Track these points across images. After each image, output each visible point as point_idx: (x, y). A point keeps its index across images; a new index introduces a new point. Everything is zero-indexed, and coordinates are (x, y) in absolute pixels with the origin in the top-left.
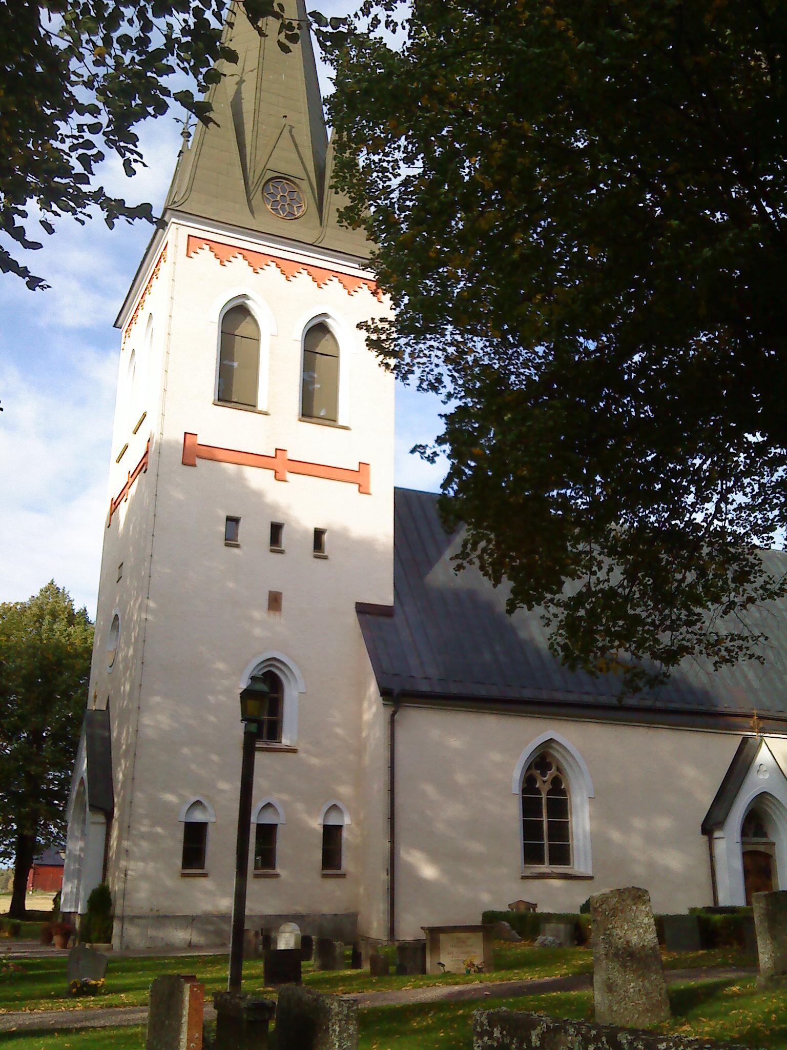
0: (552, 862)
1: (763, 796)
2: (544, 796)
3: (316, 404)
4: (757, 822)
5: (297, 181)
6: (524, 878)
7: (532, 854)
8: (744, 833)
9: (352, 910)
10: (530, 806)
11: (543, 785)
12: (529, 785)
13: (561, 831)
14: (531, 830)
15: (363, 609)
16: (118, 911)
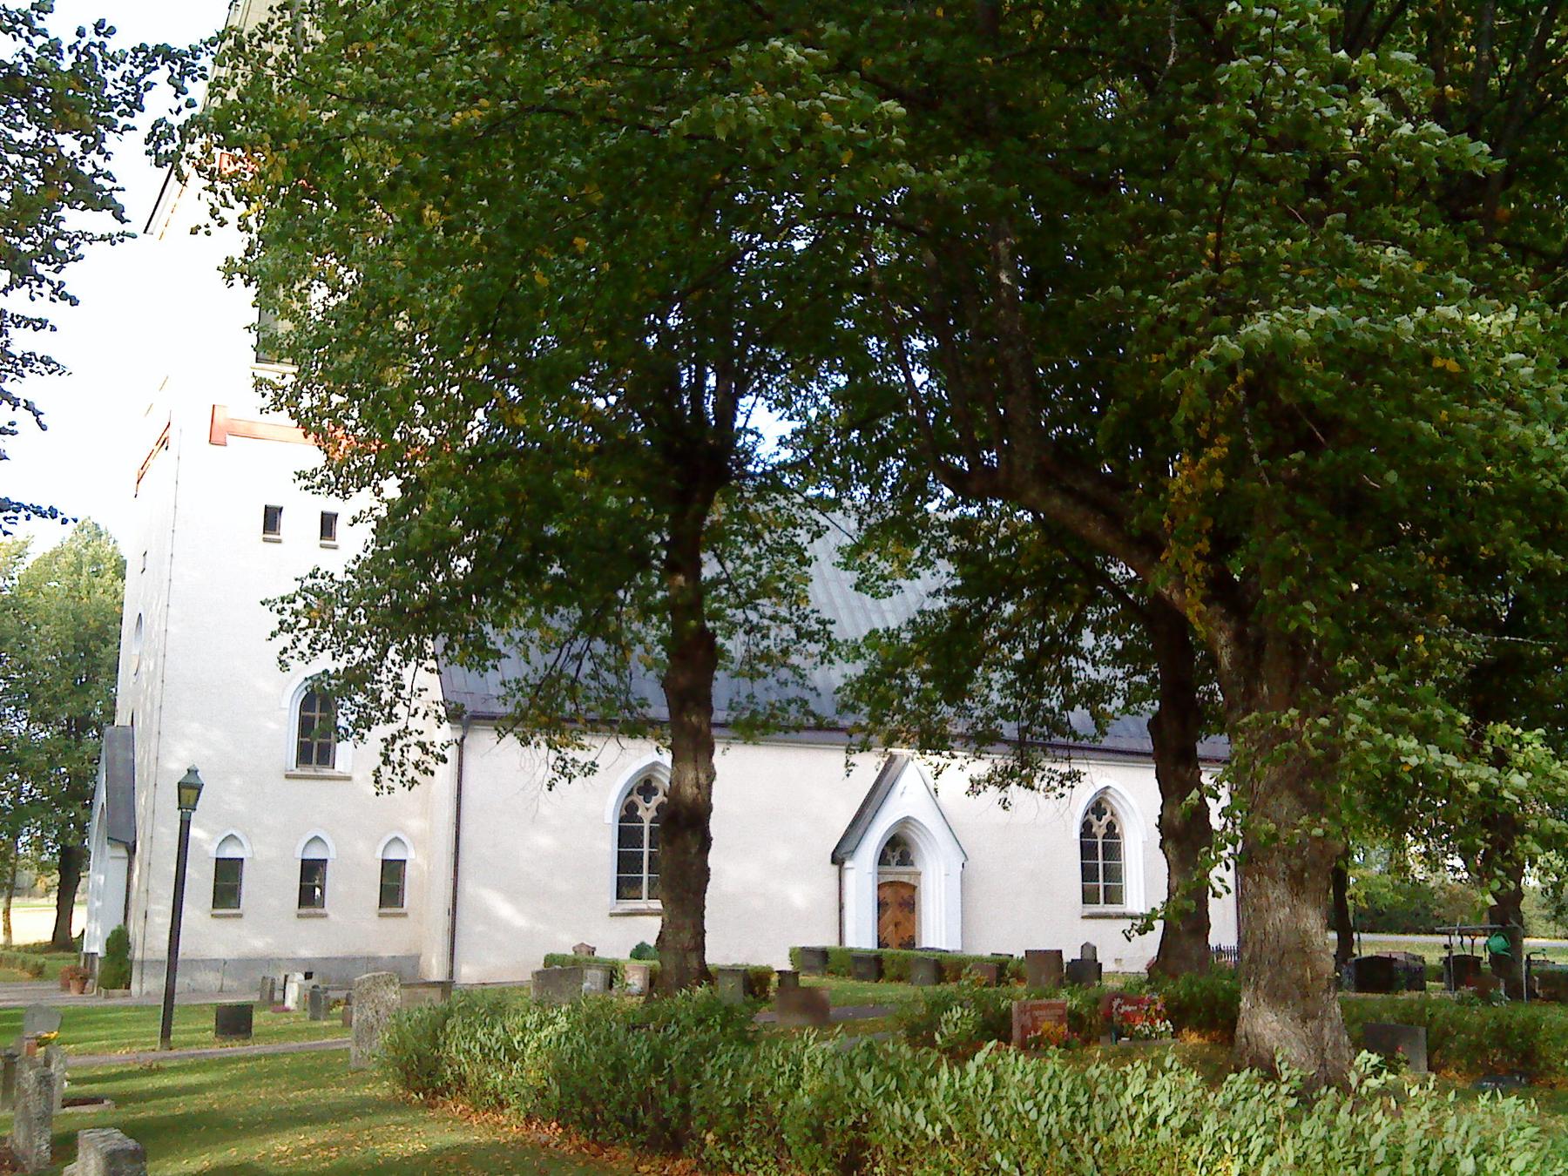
1: (906, 821)
4: (898, 848)
6: (612, 915)
7: (1088, 897)
8: (883, 860)
9: (414, 952)
10: (1087, 850)
11: (1099, 829)
12: (1086, 828)
13: (1114, 874)
14: (1088, 873)
16: (138, 955)
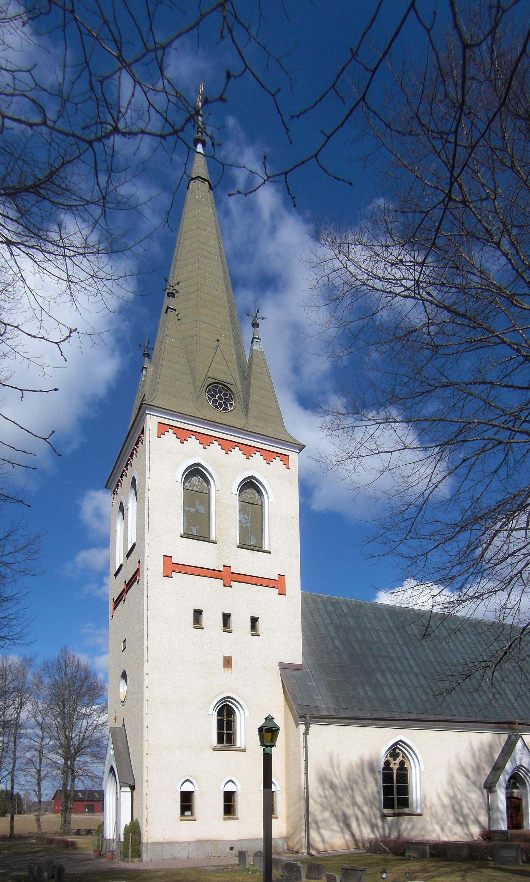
0: (102, 809)
2: (395, 772)
3: (252, 538)
4: (516, 780)
5: (229, 386)
15: (284, 667)
